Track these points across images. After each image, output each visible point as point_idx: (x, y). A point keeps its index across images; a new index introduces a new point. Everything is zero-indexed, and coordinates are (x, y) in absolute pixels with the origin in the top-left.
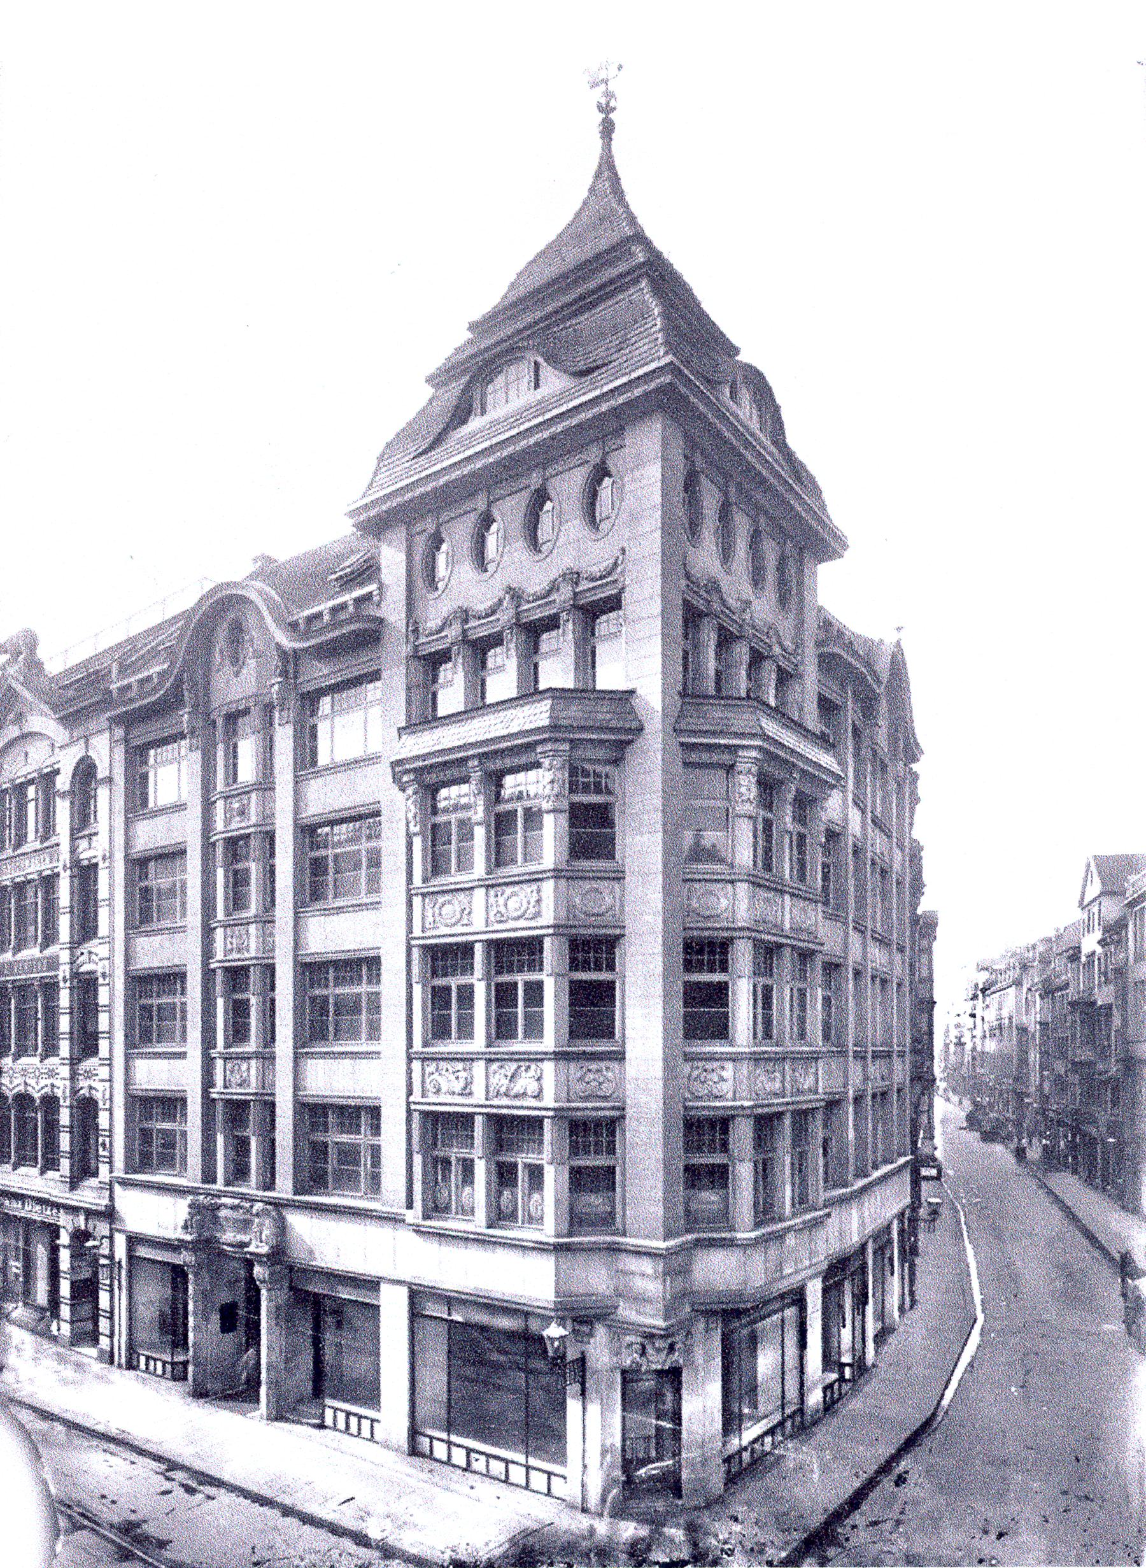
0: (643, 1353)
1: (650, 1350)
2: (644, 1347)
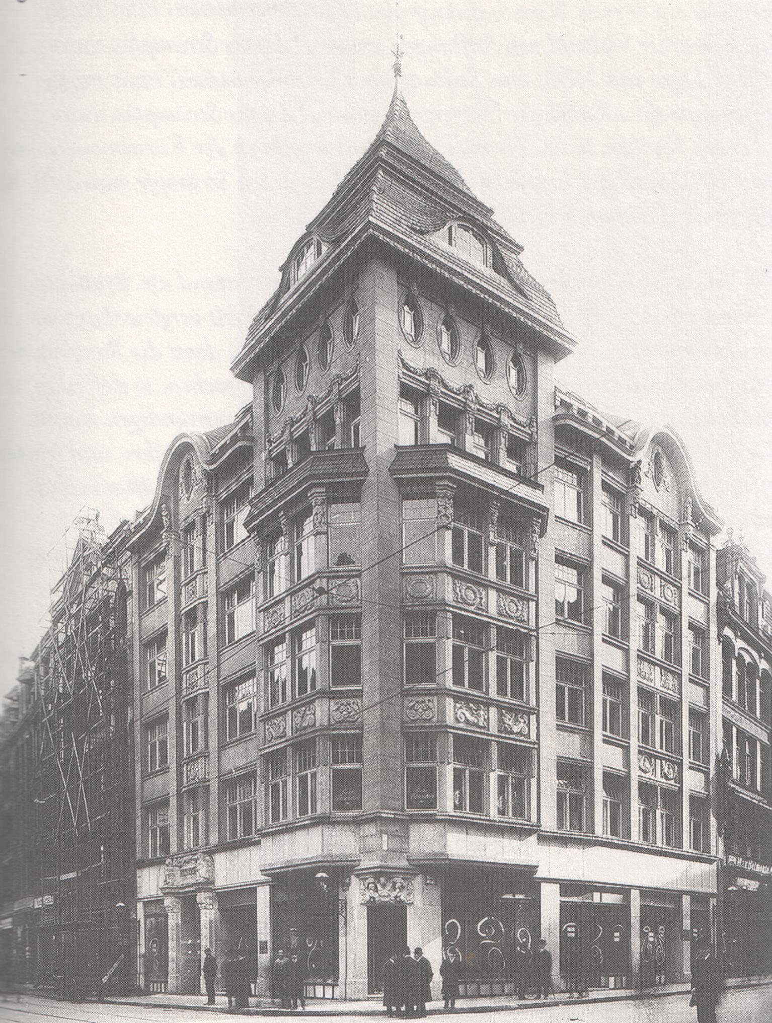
0: (376, 890)
1: (379, 888)
2: (376, 887)
